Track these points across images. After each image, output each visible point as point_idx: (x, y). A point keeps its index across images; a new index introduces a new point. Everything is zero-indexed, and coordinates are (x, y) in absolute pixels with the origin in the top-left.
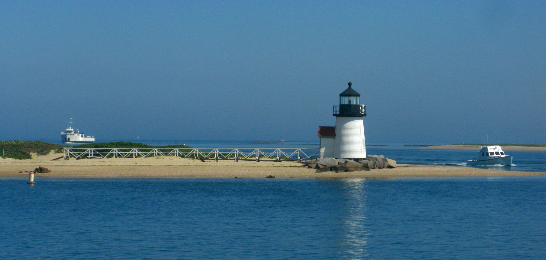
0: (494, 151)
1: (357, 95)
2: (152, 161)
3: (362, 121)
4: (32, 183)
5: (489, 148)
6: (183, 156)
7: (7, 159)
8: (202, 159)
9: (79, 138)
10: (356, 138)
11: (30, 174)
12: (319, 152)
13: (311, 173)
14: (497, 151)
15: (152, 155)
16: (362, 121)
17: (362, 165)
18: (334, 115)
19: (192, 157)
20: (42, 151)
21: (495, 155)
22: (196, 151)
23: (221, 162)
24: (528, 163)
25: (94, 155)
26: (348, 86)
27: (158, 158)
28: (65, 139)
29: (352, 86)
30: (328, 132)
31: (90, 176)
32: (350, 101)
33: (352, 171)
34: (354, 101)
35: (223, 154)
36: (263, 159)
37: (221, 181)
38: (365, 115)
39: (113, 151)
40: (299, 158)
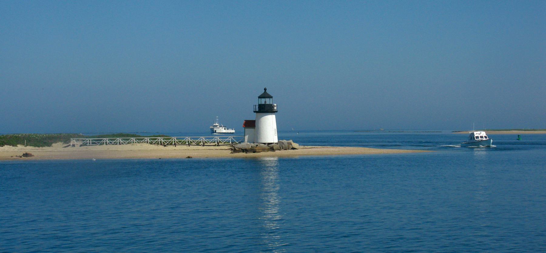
1: (270, 97)
5: (475, 133)
6: (151, 143)
7: (28, 147)
9: (223, 130)
10: (269, 128)
12: (244, 139)
14: (481, 135)
17: (271, 147)
18: (254, 112)
21: (480, 139)
23: (178, 147)
28: (213, 132)
29: (267, 91)
30: (251, 124)
32: (265, 102)
34: (268, 101)
36: (206, 144)
38: (277, 112)
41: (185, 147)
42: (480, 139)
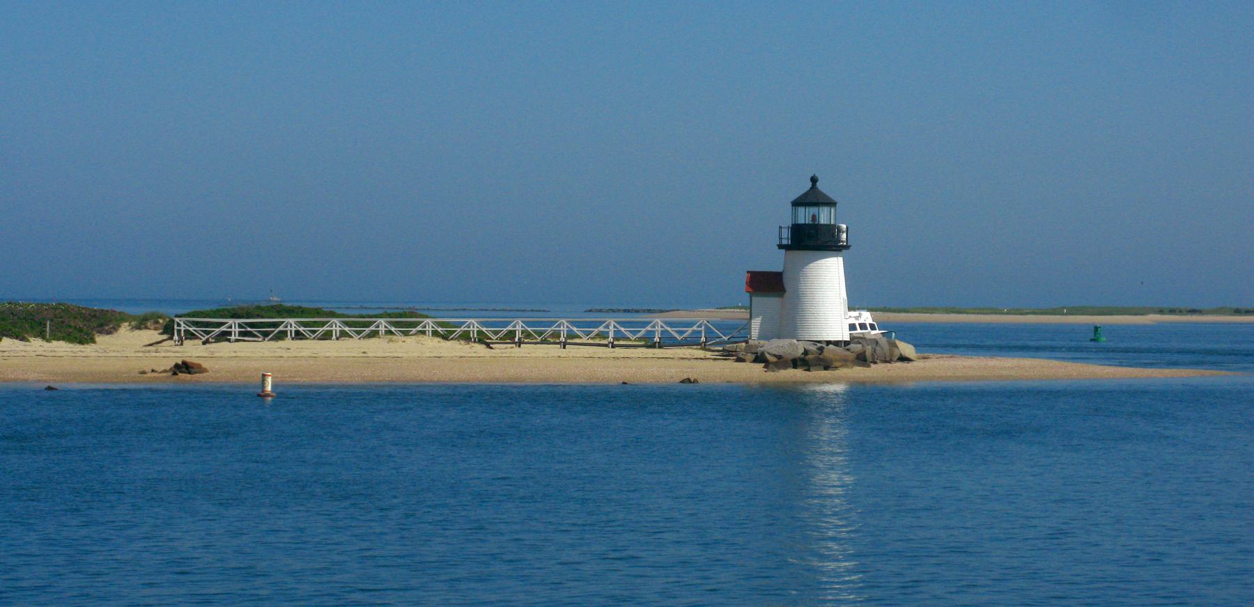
0: (857, 323)
1: (831, 203)
2: (377, 348)
3: (841, 259)
4: (268, 395)
6: (445, 337)
8: (482, 339)
10: (830, 301)
11: (264, 376)
12: (747, 327)
13: (752, 372)
14: (861, 321)
15: (374, 334)
16: (841, 259)
17: (858, 352)
18: (781, 246)
19: (465, 337)
20: (102, 325)
22: (474, 325)
24: (1126, 351)
25: (241, 334)
26: (809, 184)
27: (391, 340)
29: (818, 184)
30: (768, 284)
31: (305, 380)
33: (836, 368)
34: (825, 216)
35: (535, 332)
37: (387, 390)
38: (847, 247)
40: (703, 339)
41: (554, 350)
42: (859, 331)
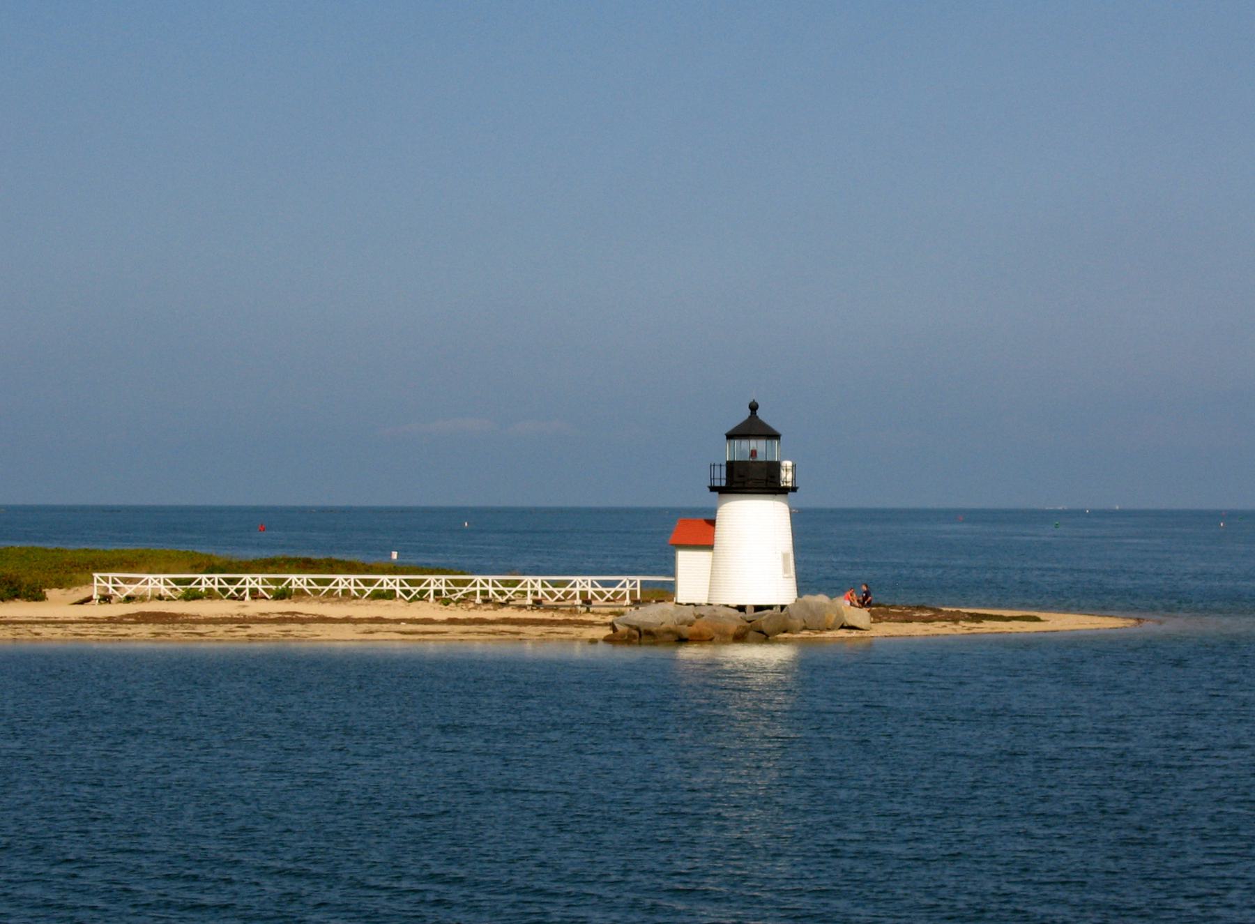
1: (773, 436)
18: (713, 489)
29: (758, 412)
32: (754, 453)
38: (794, 489)
39: (475, 585)
